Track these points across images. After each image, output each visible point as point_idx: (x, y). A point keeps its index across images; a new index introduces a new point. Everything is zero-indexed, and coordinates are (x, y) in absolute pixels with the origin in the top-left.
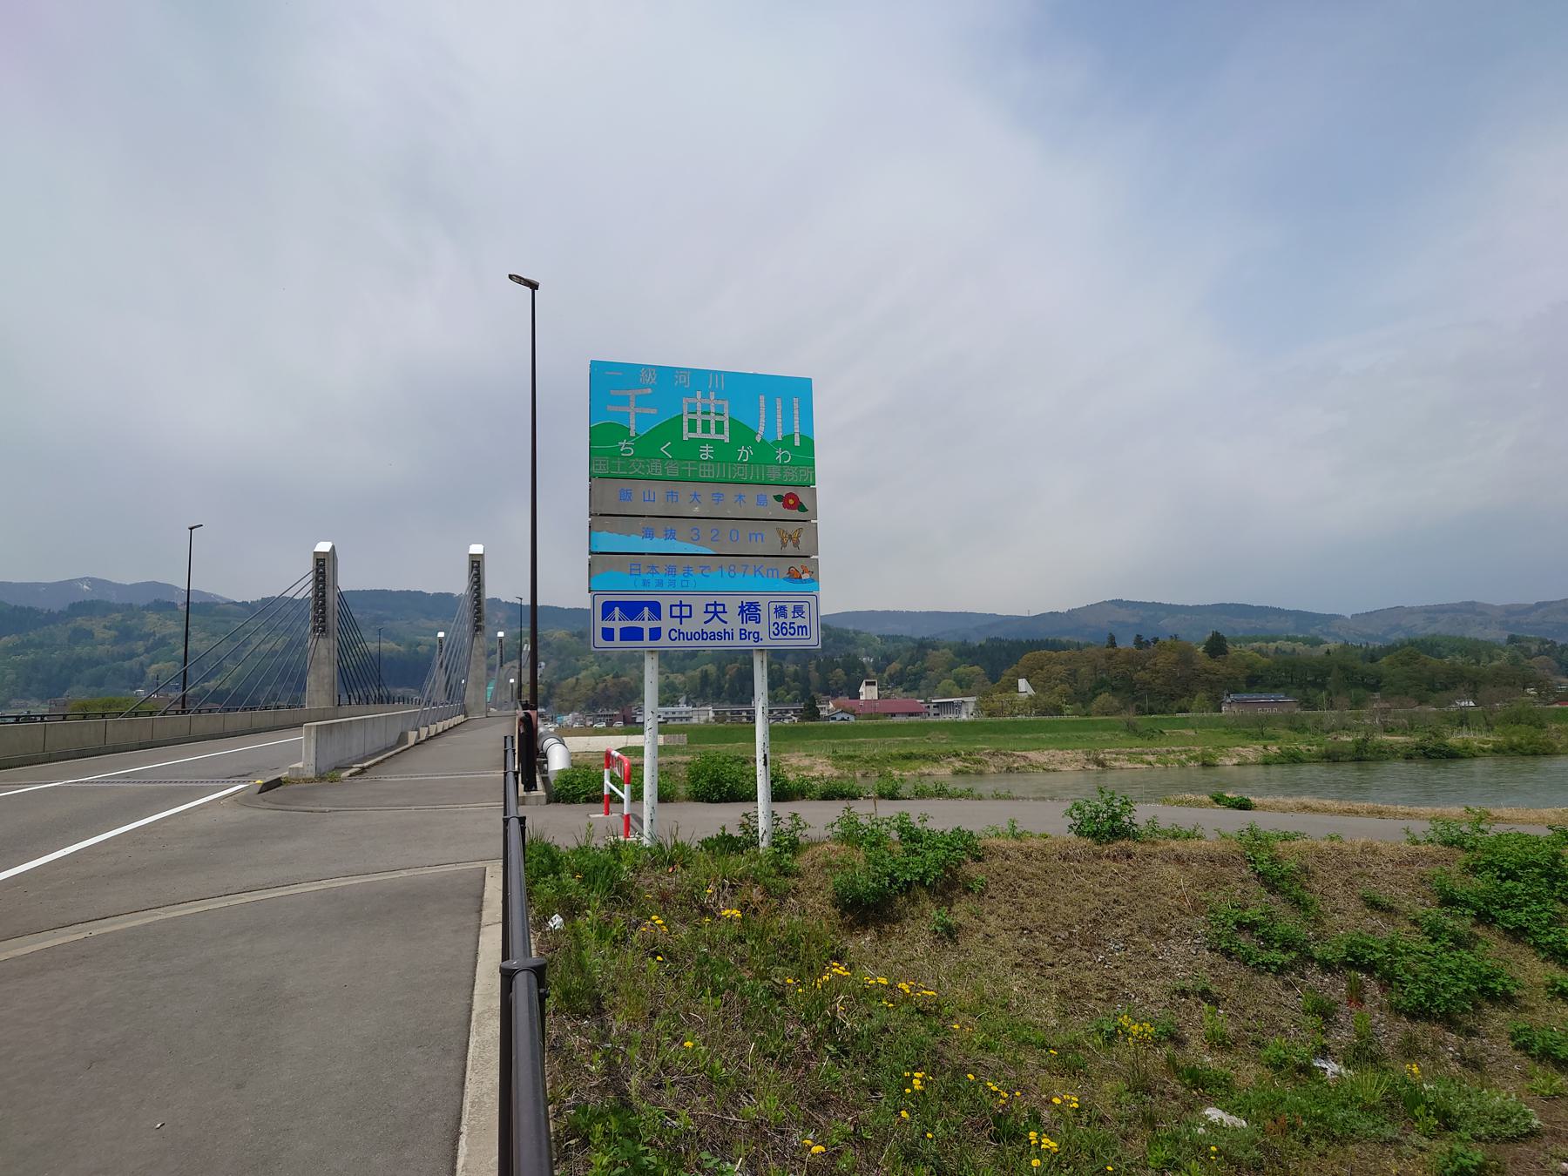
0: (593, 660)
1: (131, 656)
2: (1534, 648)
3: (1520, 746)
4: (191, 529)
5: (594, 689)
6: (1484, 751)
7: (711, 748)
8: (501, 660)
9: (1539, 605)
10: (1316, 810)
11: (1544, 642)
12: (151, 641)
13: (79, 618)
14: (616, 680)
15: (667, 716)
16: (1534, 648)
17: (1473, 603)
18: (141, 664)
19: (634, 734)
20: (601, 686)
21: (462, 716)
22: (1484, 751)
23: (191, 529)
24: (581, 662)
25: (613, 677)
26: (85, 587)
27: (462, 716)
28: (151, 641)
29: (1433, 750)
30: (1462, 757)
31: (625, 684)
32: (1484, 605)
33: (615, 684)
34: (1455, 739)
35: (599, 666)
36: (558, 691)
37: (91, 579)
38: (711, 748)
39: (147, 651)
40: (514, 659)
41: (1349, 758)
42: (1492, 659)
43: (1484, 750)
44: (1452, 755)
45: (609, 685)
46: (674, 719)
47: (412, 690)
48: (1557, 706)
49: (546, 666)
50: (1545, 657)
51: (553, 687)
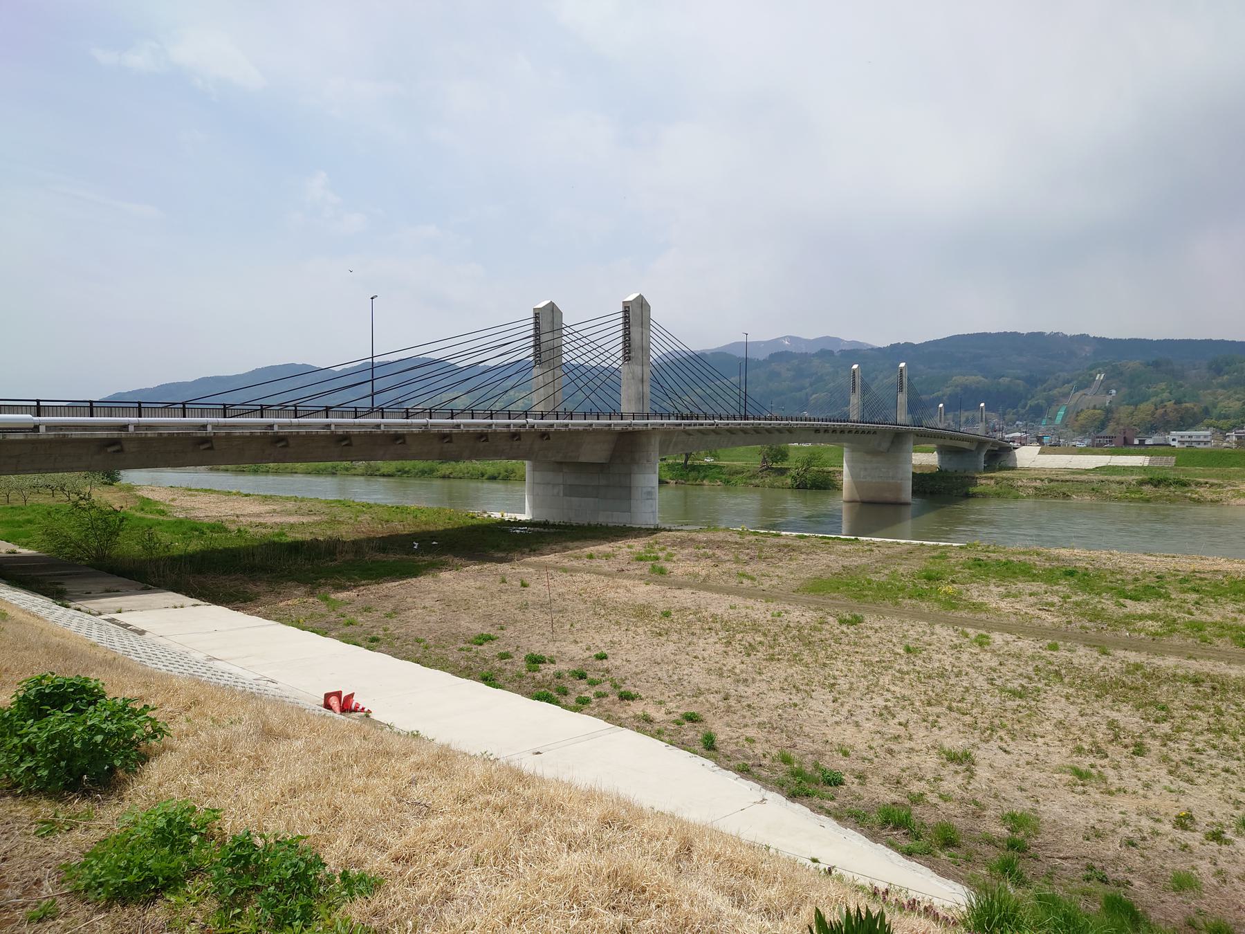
0: (1164, 387)
1: (800, 390)
4: (372, 298)
5: (1153, 413)
7: (1197, 471)
12: (814, 378)
13: (773, 364)
14: (1176, 406)
15: (1183, 440)
18: (807, 394)
19: (1119, 455)
20: (1161, 411)
21: (41, 404)
23: (372, 298)
24: (1151, 390)
25: (1175, 403)
26: (787, 342)
27: (41, 404)
28: (814, 378)
31: (1187, 409)
33: (1175, 409)
35: (1170, 393)
36: (1116, 416)
37: (790, 337)
38: (1197, 471)
39: (811, 385)
45: (1169, 410)
46: (1199, 443)
47: (993, 414)
49: (1117, 393)
51: (1112, 412)
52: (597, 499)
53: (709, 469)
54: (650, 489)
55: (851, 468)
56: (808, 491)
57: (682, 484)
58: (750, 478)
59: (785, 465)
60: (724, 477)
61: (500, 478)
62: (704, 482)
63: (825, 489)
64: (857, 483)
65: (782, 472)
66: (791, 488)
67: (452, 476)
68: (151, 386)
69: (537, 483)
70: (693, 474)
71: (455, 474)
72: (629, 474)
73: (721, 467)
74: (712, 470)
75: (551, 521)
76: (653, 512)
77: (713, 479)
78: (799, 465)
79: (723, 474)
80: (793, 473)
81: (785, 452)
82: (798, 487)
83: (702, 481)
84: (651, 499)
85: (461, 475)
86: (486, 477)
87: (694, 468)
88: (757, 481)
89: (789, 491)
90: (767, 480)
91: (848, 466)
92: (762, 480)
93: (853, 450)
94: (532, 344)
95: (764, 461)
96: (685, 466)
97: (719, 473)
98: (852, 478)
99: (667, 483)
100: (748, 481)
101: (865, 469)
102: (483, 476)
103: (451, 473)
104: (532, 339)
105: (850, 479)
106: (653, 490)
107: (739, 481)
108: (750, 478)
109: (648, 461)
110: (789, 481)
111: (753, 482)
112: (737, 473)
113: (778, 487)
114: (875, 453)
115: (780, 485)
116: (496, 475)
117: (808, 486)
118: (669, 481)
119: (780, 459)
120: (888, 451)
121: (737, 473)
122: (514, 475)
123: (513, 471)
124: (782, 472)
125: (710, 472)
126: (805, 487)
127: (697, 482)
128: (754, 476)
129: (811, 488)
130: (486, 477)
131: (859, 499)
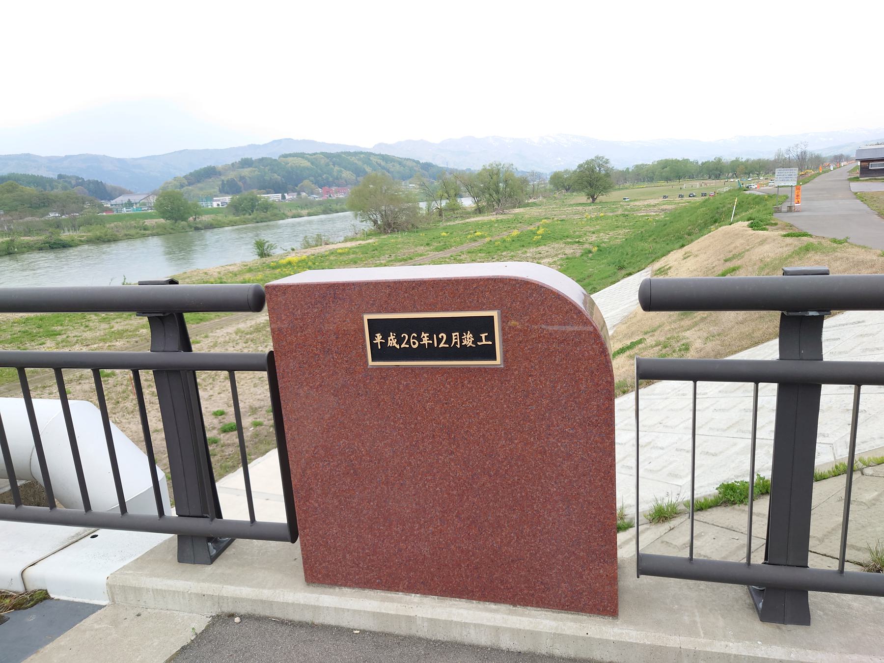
2: (73, 182)
3: (100, 237)
6: (83, 242)
8: (629, 348)
9: (67, 157)
10: (630, 302)
11: (78, 178)
16: (73, 182)
17: (28, 155)
22: (83, 242)
29: (55, 243)
30: (71, 246)
32: (35, 156)
34: (65, 235)
40: (233, 468)
41: (4, 253)
42: (52, 189)
43: (81, 241)
44: (64, 246)
48: (105, 214)
50: (80, 187)
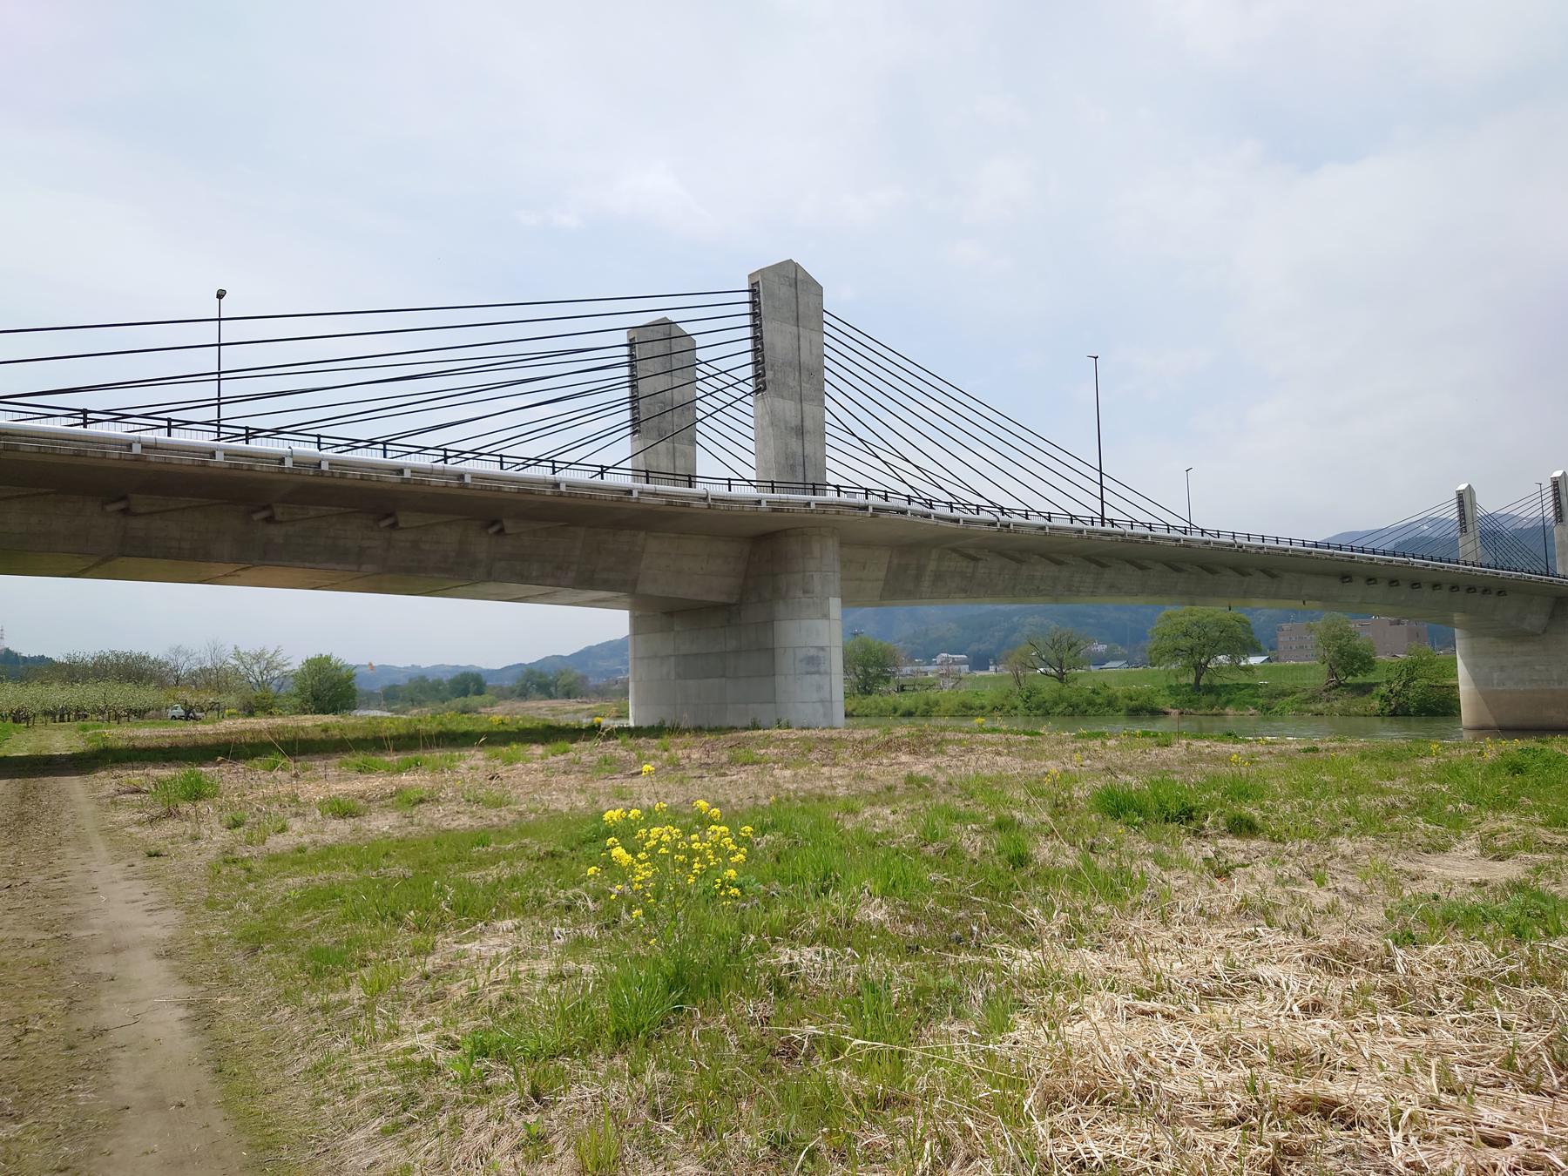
52: (724, 679)
53: (1236, 691)
54: (813, 652)
55: (1473, 668)
56: (1412, 718)
57: (1191, 714)
58: (1306, 701)
59: (1371, 678)
60: (1261, 701)
61: (918, 713)
62: (1227, 710)
63: (1445, 714)
64: (1487, 696)
65: (1365, 689)
66: (1381, 714)
67: (855, 714)
68: (620, 638)
69: (640, 658)
70: (1206, 699)
71: (859, 711)
72: (769, 623)
73: (1256, 687)
74: (1242, 692)
75: (645, 725)
76: (822, 701)
77: (1242, 705)
78: (1392, 676)
79: (1259, 697)
80: (1384, 690)
81: (1368, 657)
82: (1393, 714)
83: (1224, 709)
84: (818, 672)
85: (867, 711)
86: (899, 713)
87: (1210, 689)
88: (1320, 706)
89: (1377, 722)
90: (1337, 704)
91: (1466, 664)
92: (1328, 705)
93: (1473, 632)
94: (628, 406)
95: (1332, 673)
96: (1196, 687)
97: (1253, 696)
98: (1476, 685)
99: (1166, 713)
100: (1304, 707)
101: (1502, 669)
102: (895, 713)
103: (854, 710)
104: (628, 406)
105: (1473, 687)
106: (821, 654)
107: (1288, 708)
108: (1306, 701)
109: (805, 592)
110: (1376, 704)
111: (1312, 708)
112: (1283, 694)
113: (1357, 715)
114: (1516, 636)
115: (1362, 711)
116: (914, 710)
117: (1412, 710)
118: (1170, 710)
119: (1360, 668)
120: (1545, 631)
121: (1283, 694)
122: (937, 708)
123: (937, 703)
124: (1365, 689)
125: (1237, 695)
126: (1407, 714)
127: (1214, 711)
128: (1314, 699)
129: (1418, 713)
130: (899, 713)
131: (1493, 723)
